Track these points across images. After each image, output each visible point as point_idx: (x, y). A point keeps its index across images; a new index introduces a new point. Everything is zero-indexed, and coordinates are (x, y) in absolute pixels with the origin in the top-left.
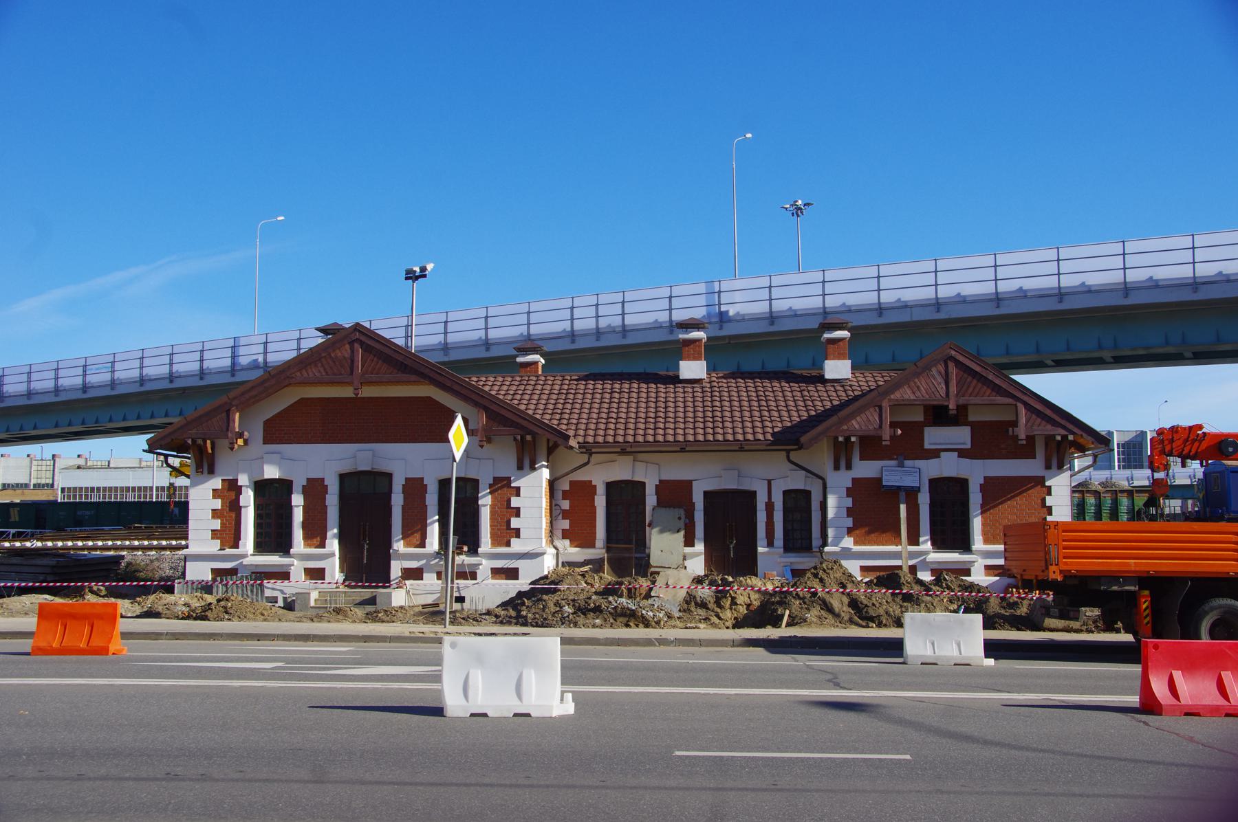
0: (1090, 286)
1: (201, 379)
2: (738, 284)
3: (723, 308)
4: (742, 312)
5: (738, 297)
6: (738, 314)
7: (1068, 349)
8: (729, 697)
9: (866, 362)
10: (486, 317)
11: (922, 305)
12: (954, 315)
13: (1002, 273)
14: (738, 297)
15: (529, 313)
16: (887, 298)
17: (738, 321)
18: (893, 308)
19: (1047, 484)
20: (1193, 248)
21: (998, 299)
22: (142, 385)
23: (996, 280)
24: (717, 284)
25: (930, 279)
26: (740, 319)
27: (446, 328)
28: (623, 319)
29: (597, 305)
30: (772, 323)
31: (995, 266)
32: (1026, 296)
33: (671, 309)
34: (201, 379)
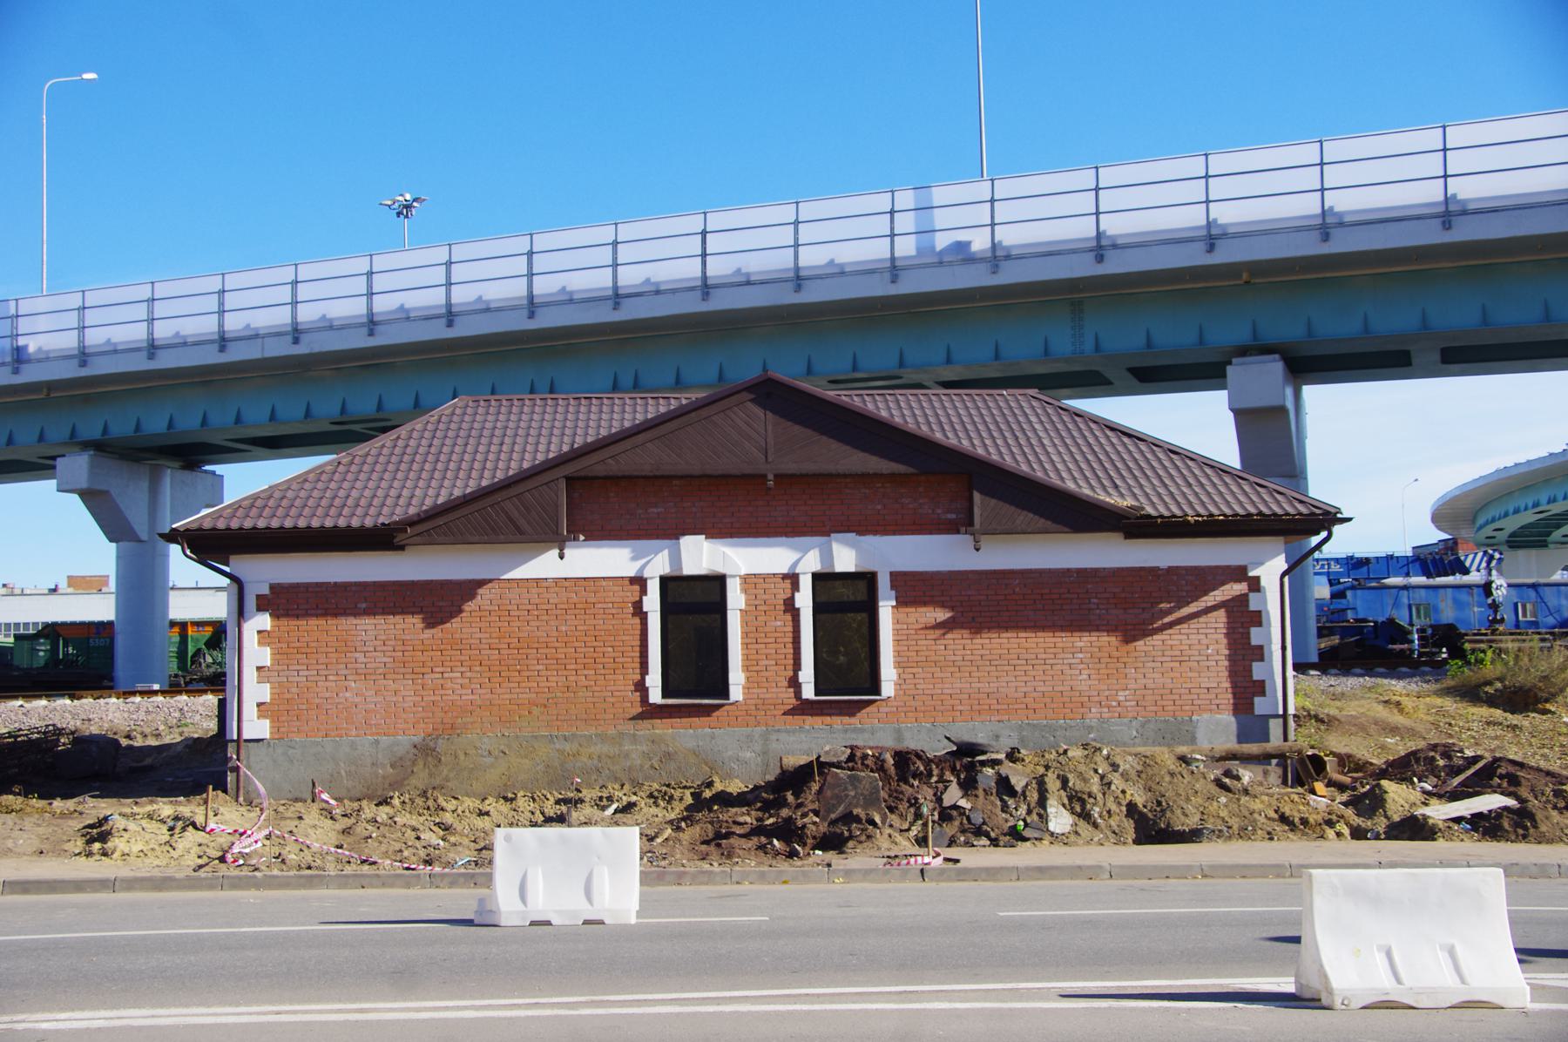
0: (841, 265)
1: (450, 324)
2: (42, 304)
3: (22, 341)
4: (45, 348)
5: (42, 323)
6: (40, 350)
7: (949, 361)
8: (1166, 978)
9: (678, 381)
10: (530, 254)
11: (592, 300)
12: (317, 349)
13: (1456, 163)
14: (42, 323)
15: (615, 244)
16: (630, 277)
17: (39, 361)
18: (733, 285)
19: (1251, 574)
20: (1445, 150)
21: (617, 297)
22: (83, 364)
23: (1322, 190)
24: (13, 304)
25: (1434, 165)
26: (45, 358)
27: (294, 293)
28: (704, 264)
29: (796, 223)
30: (83, 364)
31: (1097, 189)
32: (408, 318)
33: (449, 284)
34: (371, 334)
